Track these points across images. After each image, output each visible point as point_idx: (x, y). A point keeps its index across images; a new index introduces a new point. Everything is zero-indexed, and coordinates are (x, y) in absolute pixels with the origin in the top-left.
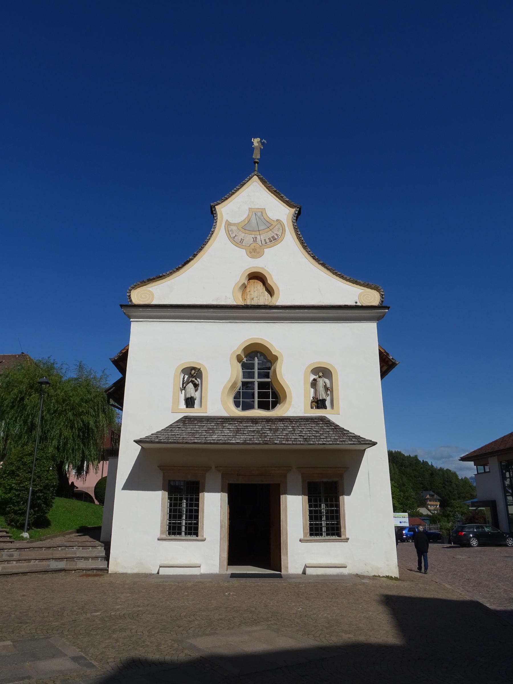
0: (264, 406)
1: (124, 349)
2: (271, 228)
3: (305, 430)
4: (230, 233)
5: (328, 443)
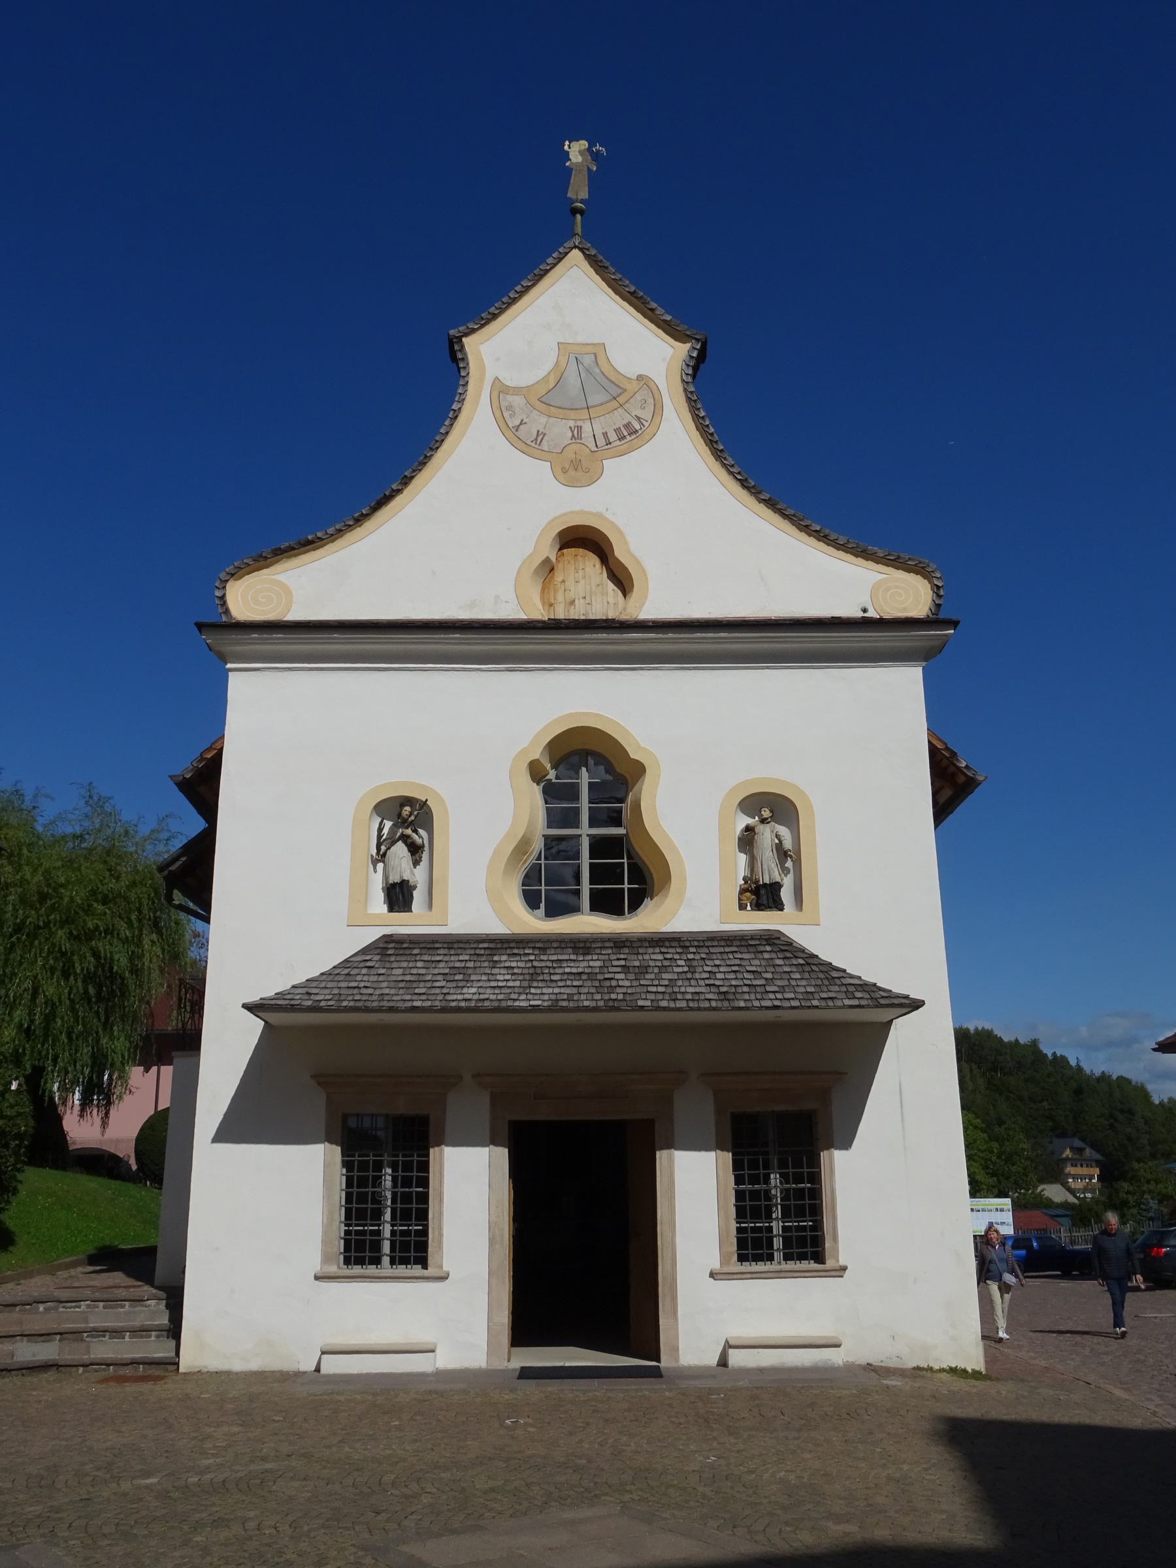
0: (606, 903)
1: (209, 749)
2: (621, 399)
3: (724, 969)
4: (506, 414)
5: (786, 1004)
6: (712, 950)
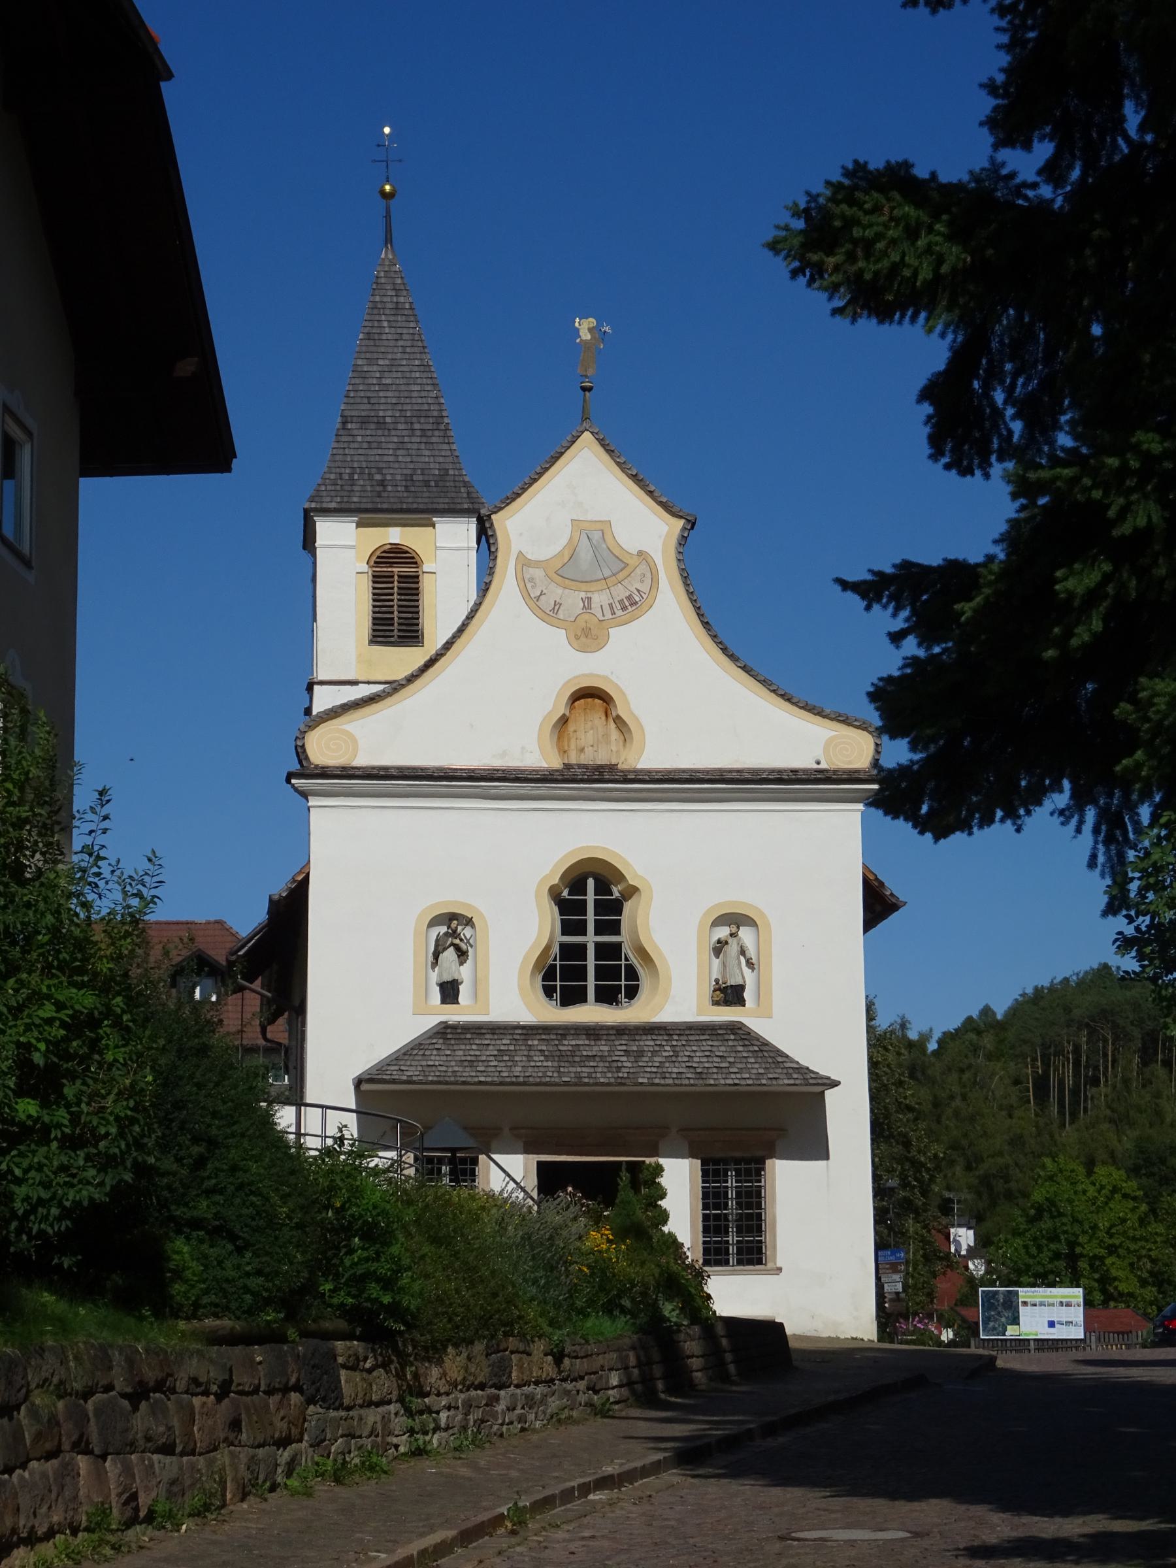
0: (607, 996)
1: (300, 872)
2: (621, 576)
3: (698, 1053)
4: (529, 586)
5: (743, 1082)
6: (691, 1038)
